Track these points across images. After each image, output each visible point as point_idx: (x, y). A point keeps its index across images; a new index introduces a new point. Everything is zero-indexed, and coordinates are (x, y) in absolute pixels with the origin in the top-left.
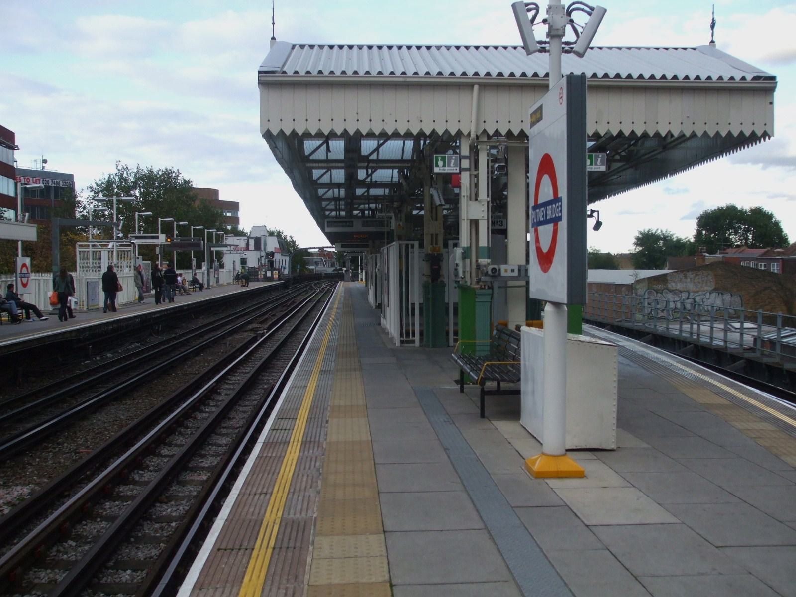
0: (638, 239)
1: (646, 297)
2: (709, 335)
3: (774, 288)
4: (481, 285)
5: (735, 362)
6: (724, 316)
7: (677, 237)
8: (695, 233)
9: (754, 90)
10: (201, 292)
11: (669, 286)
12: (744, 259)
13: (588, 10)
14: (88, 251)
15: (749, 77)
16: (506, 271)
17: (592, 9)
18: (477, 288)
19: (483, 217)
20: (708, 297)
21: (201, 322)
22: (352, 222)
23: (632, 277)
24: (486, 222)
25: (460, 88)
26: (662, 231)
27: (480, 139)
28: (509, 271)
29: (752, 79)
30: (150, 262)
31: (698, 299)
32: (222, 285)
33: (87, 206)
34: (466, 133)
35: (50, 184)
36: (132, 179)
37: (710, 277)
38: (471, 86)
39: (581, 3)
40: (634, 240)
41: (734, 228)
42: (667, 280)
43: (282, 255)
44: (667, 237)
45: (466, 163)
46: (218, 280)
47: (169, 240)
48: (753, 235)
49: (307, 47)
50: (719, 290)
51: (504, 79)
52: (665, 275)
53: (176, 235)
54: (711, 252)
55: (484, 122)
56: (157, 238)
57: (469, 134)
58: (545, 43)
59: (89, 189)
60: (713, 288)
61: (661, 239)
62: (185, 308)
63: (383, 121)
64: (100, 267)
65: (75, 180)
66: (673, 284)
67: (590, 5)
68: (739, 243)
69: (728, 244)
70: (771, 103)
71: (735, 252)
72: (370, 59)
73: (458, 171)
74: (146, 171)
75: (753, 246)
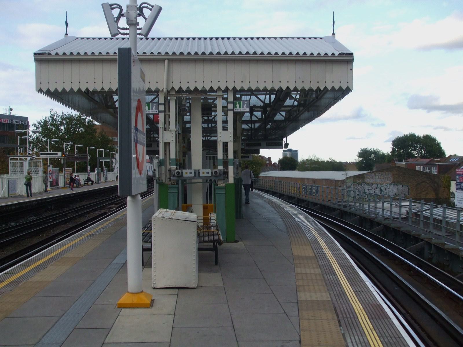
0: (360, 153)
1: (352, 187)
2: (389, 209)
3: (428, 182)
4: (172, 183)
5: (378, 226)
6: (396, 199)
7: (382, 152)
8: (391, 150)
9: (325, 61)
10: (92, 186)
11: (366, 181)
12: (418, 165)
13: (150, 7)
14: (17, 162)
15: (337, 54)
16: (186, 173)
17: (152, 6)
18: (169, 184)
19: (173, 140)
20: (388, 187)
21: (83, 203)
22: (151, 144)
23: (344, 176)
24: (175, 143)
25: (157, 62)
26: (374, 149)
27: (171, 93)
28: (189, 173)
29: (339, 55)
30: (58, 168)
31: (382, 188)
32: (109, 181)
33: (32, 136)
34: (161, 90)
35: (14, 123)
36: (59, 119)
37: (390, 175)
38: (163, 60)
39: (146, 3)
40: (357, 154)
41: (414, 147)
42: (364, 177)
43: (151, 164)
44: (377, 152)
45: (162, 108)
46: (106, 179)
47: (63, 155)
48: (425, 151)
49: (174, 39)
50: (395, 183)
51: (199, 56)
52: (364, 174)
53: (77, 152)
54: (400, 161)
55: (173, 82)
56: (57, 154)
57: (163, 90)
58: (127, 29)
59: (34, 126)
60: (391, 182)
61: (373, 153)
62: (72, 195)
63: (110, 82)
64: (23, 171)
65: (29, 120)
66: (368, 180)
67: (152, 4)
68: (417, 156)
69: (412, 156)
70: (351, 69)
71: (413, 161)
72: (212, 46)
73: (157, 113)
74: (67, 115)
75: (422, 157)
